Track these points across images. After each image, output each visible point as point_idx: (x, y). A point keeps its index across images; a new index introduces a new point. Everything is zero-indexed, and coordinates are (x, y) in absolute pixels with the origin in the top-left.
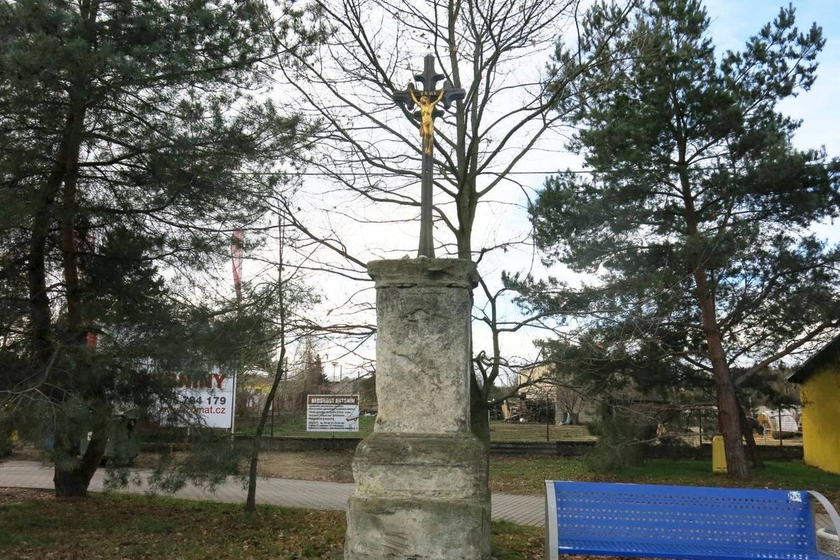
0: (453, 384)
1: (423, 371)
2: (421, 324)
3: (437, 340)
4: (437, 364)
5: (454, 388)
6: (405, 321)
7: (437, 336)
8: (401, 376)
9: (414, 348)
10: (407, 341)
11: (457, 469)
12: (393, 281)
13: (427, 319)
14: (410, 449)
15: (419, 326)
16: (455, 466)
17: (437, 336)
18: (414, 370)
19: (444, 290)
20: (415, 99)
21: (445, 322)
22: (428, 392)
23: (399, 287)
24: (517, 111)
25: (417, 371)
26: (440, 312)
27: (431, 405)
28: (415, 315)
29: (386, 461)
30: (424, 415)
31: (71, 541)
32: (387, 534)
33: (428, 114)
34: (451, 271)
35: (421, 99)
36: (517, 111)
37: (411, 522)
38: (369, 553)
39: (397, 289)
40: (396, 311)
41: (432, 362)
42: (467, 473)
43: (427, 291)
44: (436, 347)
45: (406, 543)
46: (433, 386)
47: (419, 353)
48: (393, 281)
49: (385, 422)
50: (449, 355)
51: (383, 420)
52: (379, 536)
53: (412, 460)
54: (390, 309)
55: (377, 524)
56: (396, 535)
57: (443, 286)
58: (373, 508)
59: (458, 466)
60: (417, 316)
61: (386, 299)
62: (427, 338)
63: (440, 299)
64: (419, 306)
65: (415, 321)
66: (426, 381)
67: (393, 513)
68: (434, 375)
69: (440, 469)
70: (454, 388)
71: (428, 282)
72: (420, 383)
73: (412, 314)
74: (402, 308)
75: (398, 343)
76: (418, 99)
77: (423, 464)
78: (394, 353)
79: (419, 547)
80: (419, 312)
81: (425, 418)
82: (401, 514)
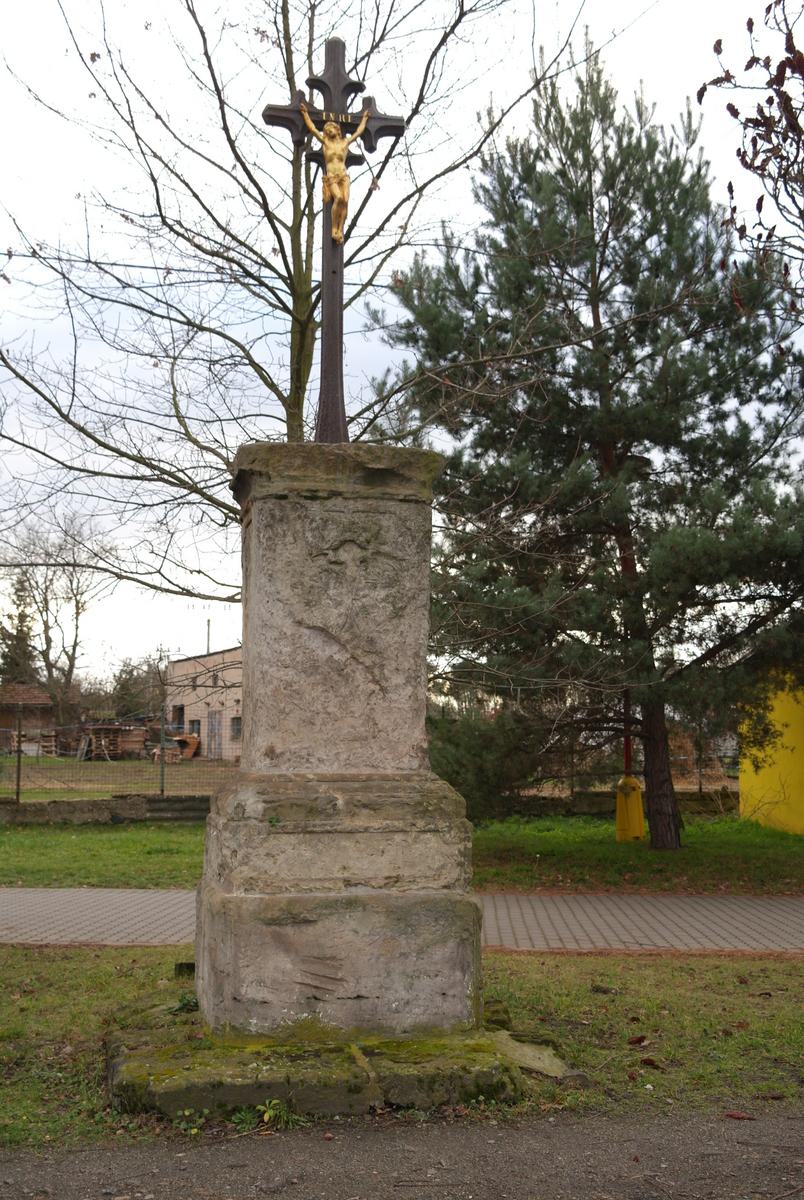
0: (408, 682)
1: (353, 657)
2: (352, 570)
3: (383, 600)
4: (380, 645)
5: (409, 690)
6: (322, 561)
7: (383, 593)
8: (312, 668)
9: (340, 615)
10: (325, 601)
11: (428, 835)
12: (296, 484)
13: (363, 561)
14: (340, 802)
15: (348, 573)
16: (425, 832)
17: (383, 593)
18: (336, 657)
19: (392, 505)
20: (312, 126)
21: (397, 566)
22: (362, 698)
23: (306, 498)
24: (216, 165)
25: (341, 657)
26: (385, 548)
27: (370, 719)
28: (341, 551)
29: (296, 827)
30: (355, 740)
31: (254, 1179)
32: (303, 961)
33: (341, 159)
34: (407, 473)
35: (327, 127)
36: (216, 165)
37: (350, 936)
38: (269, 997)
39: (302, 501)
40: (301, 543)
41: (371, 641)
42: (445, 843)
43: (361, 508)
44: (382, 613)
45: (340, 975)
46: (372, 686)
47: (350, 624)
48: (296, 484)
49: (282, 753)
50: (402, 628)
51: (278, 751)
52: (289, 966)
53: (348, 823)
54: (290, 539)
55: (284, 944)
56: (321, 959)
57: (392, 498)
58: (277, 914)
59: (429, 831)
60: (344, 555)
61: (281, 520)
62: (364, 596)
63: (385, 523)
64: (348, 536)
65: (342, 563)
66: (360, 676)
67: (315, 921)
68: (375, 664)
69: (398, 837)
70: (409, 690)
71: (361, 488)
72: (347, 678)
73: (336, 549)
74: (314, 537)
75: (308, 604)
76: (320, 125)
77: (366, 830)
78: (300, 623)
79: (363, 981)
80: (347, 547)
81: (357, 745)
82: (331, 923)
